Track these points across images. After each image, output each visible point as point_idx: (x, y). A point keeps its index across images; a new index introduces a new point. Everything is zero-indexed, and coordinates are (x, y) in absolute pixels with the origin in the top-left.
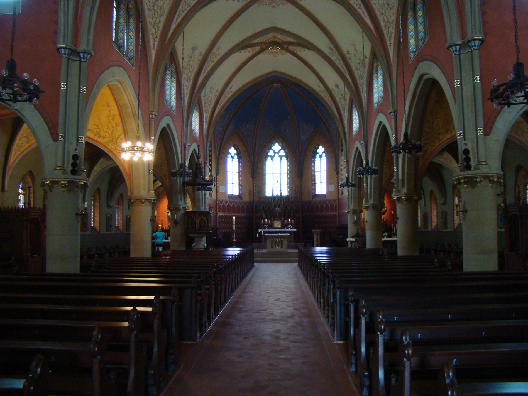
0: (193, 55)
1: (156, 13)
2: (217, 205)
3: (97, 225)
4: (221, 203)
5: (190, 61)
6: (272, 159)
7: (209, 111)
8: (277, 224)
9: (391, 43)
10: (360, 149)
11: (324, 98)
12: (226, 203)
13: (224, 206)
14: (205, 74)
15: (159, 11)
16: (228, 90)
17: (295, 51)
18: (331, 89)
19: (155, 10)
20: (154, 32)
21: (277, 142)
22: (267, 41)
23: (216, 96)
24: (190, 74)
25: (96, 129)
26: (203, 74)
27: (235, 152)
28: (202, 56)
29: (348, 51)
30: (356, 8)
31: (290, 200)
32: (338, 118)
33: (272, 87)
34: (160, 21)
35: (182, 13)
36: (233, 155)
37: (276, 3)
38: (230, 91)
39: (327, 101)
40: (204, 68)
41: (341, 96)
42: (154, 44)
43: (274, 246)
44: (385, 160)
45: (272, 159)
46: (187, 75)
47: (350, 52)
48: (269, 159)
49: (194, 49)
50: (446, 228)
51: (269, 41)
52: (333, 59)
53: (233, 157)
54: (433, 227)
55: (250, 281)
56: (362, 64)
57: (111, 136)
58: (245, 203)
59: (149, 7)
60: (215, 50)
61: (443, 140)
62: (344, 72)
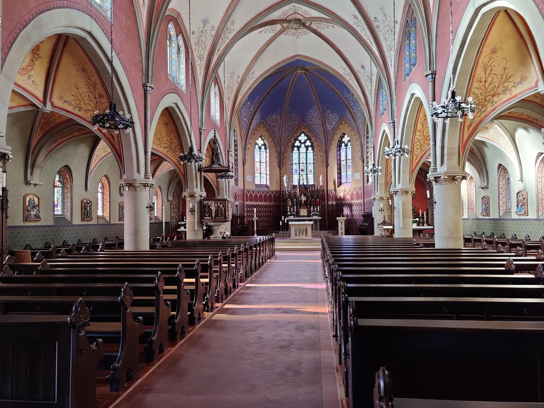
0: (205, 29)
2: (244, 195)
3: (107, 215)
4: (249, 192)
5: (201, 36)
6: (298, 150)
8: (304, 212)
10: (387, 131)
11: (350, 82)
12: (254, 192)
13: (251, 195)
14: (220, 52)
16: (250, 76)
17: (318, 30)
18: (357, 71)
23: (238, 82)
25: (74, 100)
29: (375, 18)
31: (316, 189)
33: (296, 74)
38: (252, 77)
39: (352, 84)
41: (367, 78)
43: (298, 235)
44: (416, 140)
45: (298, 150)
47: (378, 19)
48: (296, 149)
50: (488, 215)
52: (358, 29)
53: (260, 148)
55: (261, 274)
56: (392, 31)
58: (272, 192)
61: (498, 103)
62: (370, 44)
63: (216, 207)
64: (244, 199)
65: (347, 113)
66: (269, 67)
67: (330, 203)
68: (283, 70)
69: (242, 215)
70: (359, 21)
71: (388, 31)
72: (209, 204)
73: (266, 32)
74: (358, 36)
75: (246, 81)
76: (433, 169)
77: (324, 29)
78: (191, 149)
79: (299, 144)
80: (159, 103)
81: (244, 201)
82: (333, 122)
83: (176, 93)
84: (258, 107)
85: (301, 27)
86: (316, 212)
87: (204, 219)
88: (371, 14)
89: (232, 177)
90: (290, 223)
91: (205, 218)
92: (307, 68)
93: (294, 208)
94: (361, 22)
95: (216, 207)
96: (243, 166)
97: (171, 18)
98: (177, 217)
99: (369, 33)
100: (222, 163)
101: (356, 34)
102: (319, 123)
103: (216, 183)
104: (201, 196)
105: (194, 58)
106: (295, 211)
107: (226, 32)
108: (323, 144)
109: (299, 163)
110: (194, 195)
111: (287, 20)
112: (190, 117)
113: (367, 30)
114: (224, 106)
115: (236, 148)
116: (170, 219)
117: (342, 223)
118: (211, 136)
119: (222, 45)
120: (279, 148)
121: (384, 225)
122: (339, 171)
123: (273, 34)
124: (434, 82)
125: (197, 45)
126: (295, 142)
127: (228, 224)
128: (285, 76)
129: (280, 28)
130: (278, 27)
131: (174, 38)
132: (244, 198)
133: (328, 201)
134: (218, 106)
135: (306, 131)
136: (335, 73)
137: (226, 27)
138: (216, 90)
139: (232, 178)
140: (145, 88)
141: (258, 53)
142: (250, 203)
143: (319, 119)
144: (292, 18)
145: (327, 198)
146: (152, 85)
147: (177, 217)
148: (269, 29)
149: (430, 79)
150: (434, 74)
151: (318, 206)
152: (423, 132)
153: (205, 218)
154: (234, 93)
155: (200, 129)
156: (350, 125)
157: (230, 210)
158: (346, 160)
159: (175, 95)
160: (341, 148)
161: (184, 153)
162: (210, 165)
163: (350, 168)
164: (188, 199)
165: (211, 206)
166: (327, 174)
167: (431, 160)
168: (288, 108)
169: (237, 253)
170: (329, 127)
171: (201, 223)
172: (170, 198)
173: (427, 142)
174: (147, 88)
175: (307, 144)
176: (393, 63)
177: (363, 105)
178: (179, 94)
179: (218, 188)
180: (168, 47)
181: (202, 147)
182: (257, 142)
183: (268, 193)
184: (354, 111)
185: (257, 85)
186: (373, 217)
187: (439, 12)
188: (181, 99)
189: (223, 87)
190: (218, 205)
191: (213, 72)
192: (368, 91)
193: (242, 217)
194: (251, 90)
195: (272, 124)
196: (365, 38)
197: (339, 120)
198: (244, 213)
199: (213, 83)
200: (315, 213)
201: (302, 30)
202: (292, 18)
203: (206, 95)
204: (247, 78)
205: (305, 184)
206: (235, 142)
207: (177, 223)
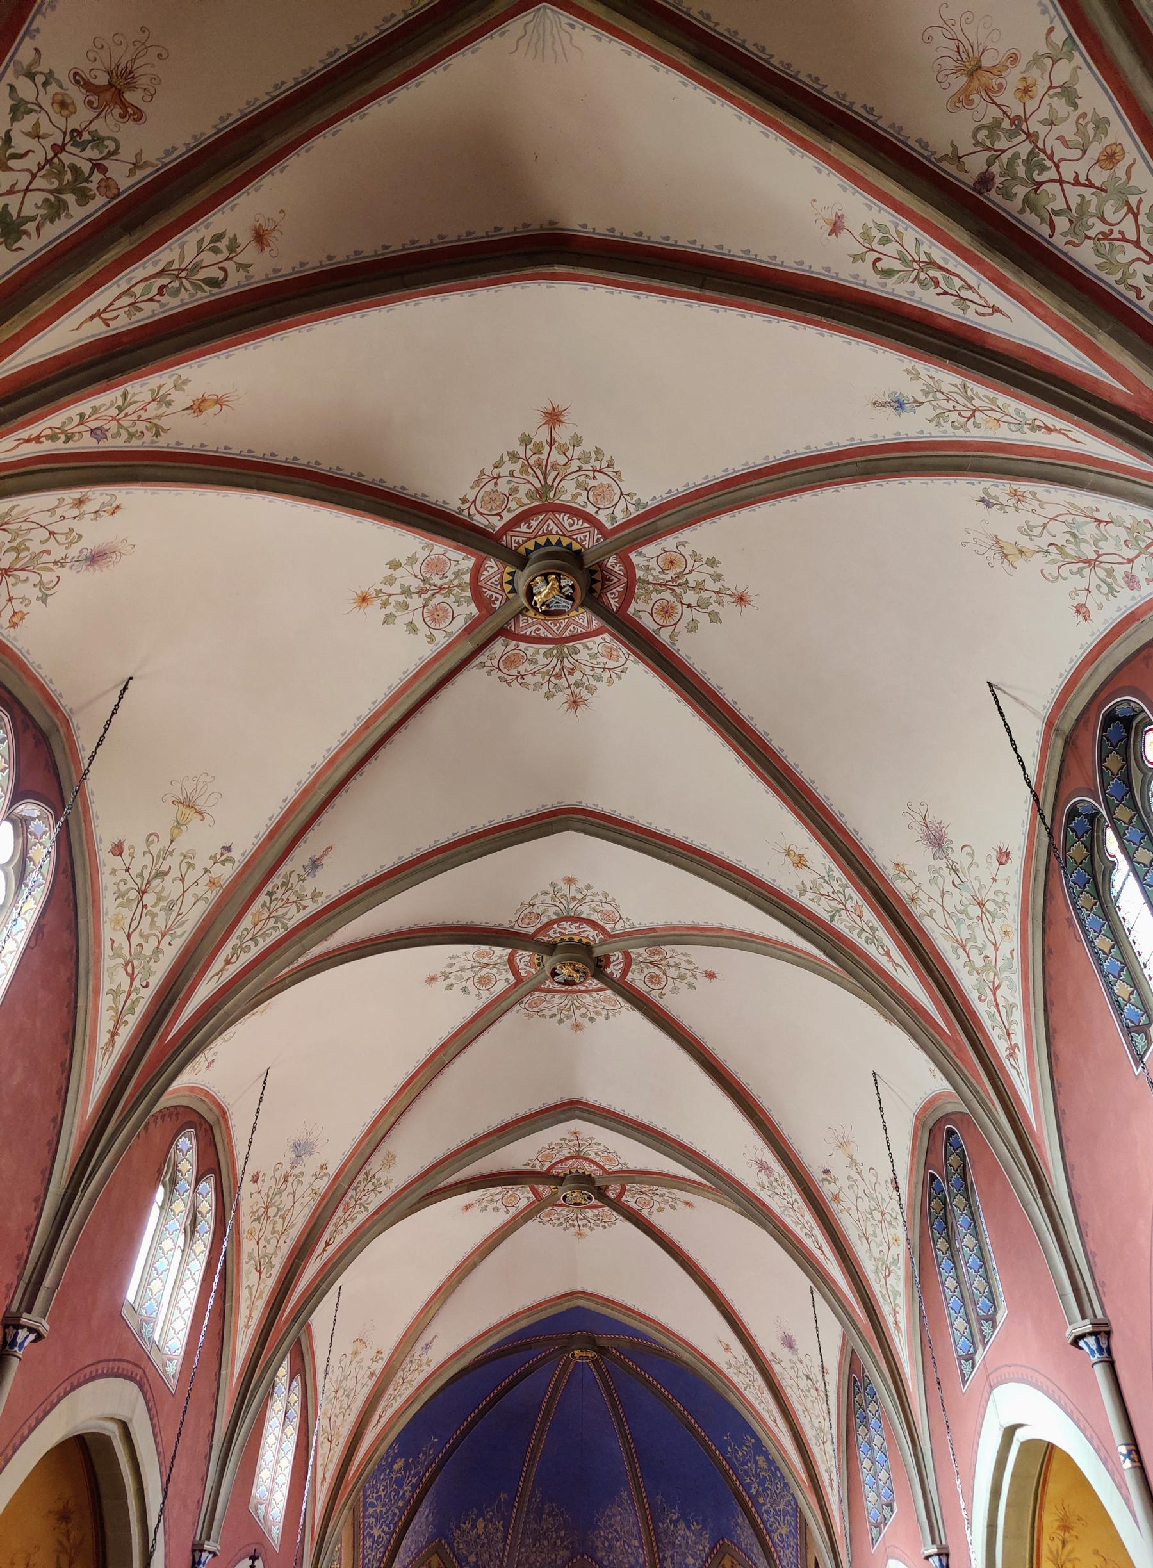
0: (296, 1171)
1: (146, 920)
5: (280, 1192)
7: (339, 1435)
9: (1017, 1045)
14: (331, 1249)
15: (162, 916)
16: (417, 1357)
17: (645, 1213)
18: (769, 1357)
20: (125, 986)
23: (372, 1374)
26: (324, 1250)
29: (826, 1172)
30: (861, 942)
32: (803, 1475)
34: (158, 950)
35: (252, 943)
37: (583, 1010)
38: (425, 1358)
39: (756, 1404)
41: (804, 1383)
42: (114, 1034)
46: (332, 1420)
49: (301, 1149)
59: (123, 888)
62: (817, 1253)
65: (737, 1524)
66: (484, 1327)
68: (529, 1343)
70: (776, 1180)
73: (485, 1208)
74: (776, 1227)
75: (400, 1373)
77: (661, 1210)
80: (53, 1406)
84: (431, 1480)
85: (594, 1201)
88: (813, 1158)
92: (603, 1343)
94: (783, 1183)
97: (194, 1118)
99: (809, 1218)
101: (771, 1221)
102: (641, 1561)
105: (239, 1263)
111: (553, 1176)
113: (804, 1206)
114: (311, 1460)
123: (507, 1217)
124: (1111, 1365)
125: (259, 1218)
128: (530, 1367)
129: (528, 1198)
130: (523, 1196)
131: (185, 1183)
136: (699, 1360)
137: (363, 1172)
138: (293, 1398)
140: (11, 1331)
141: (451, 1276)
143: (640, 1542)
146: (44, 1323)
148: (496, 1198)
149: (1092, 1351)
150: (1102, 1333)
154: (351, 1418)
155: (197, 1549)
159: (131, 1388)
168: (533, 1495)
174: (16, 1334)
176: (902, 1318)
178: (146, 1387)
180: (155, 1212)
184: (765, 1516)
185: (434, 1391)
187: (1062, 1124)
188: (149, 1409)
189: (320, 1389)
191: (295, 1320)
192: (814, 1432)
196: (801, 1233)
199: (286, 1363)
201: (598, 1212)
202: (568, 1172)
204: (408, 1360)
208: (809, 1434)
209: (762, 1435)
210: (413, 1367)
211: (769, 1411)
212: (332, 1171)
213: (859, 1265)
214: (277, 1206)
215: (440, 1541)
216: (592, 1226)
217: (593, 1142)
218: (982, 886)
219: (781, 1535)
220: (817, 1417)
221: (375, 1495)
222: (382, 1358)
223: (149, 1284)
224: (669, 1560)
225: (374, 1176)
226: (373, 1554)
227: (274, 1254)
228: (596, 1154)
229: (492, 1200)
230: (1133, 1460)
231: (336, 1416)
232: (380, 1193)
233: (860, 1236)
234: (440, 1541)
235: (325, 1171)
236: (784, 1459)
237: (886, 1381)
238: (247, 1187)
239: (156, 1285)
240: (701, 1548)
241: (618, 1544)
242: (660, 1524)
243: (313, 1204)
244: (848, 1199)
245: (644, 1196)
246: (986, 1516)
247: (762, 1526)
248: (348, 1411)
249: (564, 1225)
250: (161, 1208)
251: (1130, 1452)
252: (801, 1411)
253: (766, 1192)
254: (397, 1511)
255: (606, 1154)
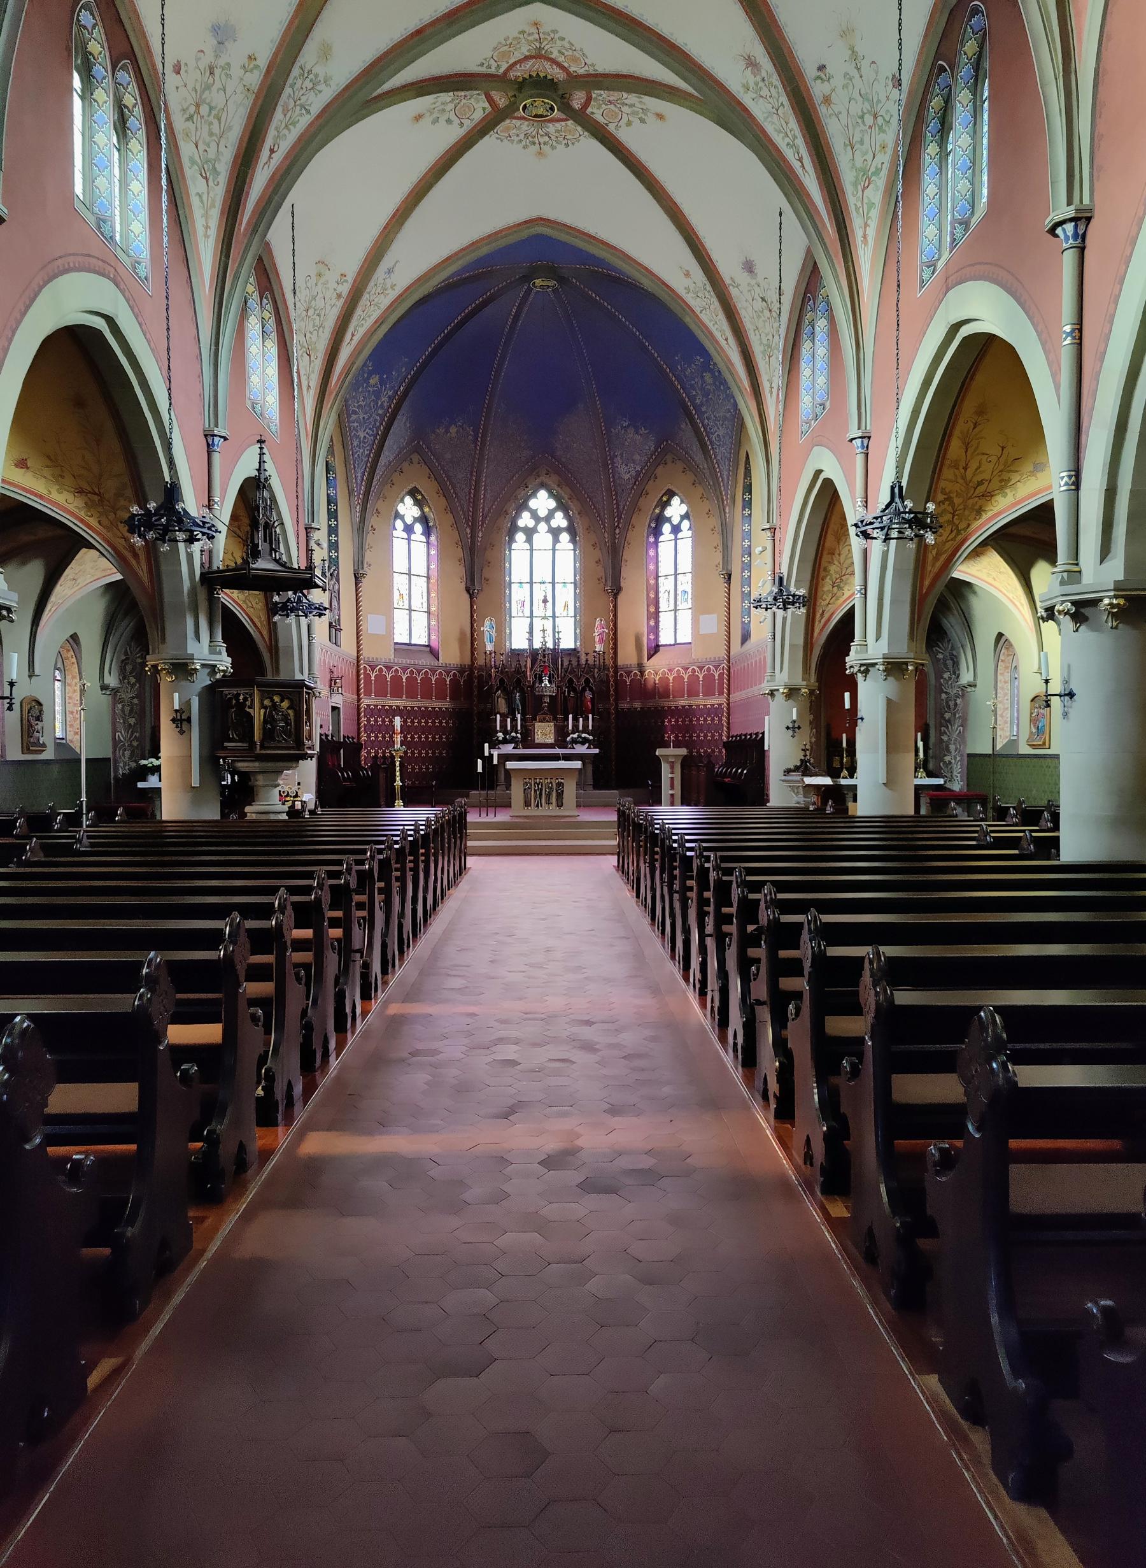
2: (358, 675)
5: (208, 87)
6: (529, 540)
8: (544, 732)
11: (703, 316)
13: (381, 677)
14: (278, 157)
16: (381, 281)
17: (611, 128)
18: (728, 281)
19: (202, 117)
21: (543, 486)
22: (512, 75)
23: (339, 296)
24: (213, 145)
27: (416, 512)
28: (256, 72)
29: (822, 68)
31: (583, 662)
33: (529, 290)
36: (409, 521)
38: (389, 283)
39: (710, 325)
40: (271, 133)
41: (759, 304)
45: (529, 540)
48: (520, 537)
49: (222, 33)
51: (519, 73)
53: (409, 529)
54: (999, 747)
57: (96, 490)
60: (309, 55)
62: (796, 165)
63: (266, 708)
64: (358, 690)
67: (624, 705)
69: (353, 738)
71: (864, 114)
72: (241, 697)
76: (1065, 574)
78: (172, 492)
79: (531, 523)
81: (358, 695)
82: (637, 457)
83: (109, 278)
84: (405, 394)
86: (583, 732)
87: (225, 748)
88: (807, 57)
89: (320, 611)
90: (510, 765)
91: (226, 744)
93: (514, 720)
94: (771, 83)
95: (266, 708)
96: (356, 584)
98: (135, 744)
100: (284, 558)
103: (265, 633)
104: (213, 669)
106: (519, 728)
107: (299, 82)
108: (603, 523)
109: (531, 583)
110: (186, 664)
112: (166, 374)
113: (791, 112)
115: (333, 523)
116: (111, 750)
117: (672, 768)
118: (246, 467)
119: (286, 132)
120: (468, 531)
121: (804, 775)
122: (652, 610)
123: (462, 132)
124: (1082, 250)
125: (191, 117)
126: (518, 515)
127: (308, 769)
130: (477, 106)
132: (358, 686)
133: (617, 700)
134: (273, 370)
135: (552, 480)
138: (267, 315)
139: (320, 615)
142: (380, 702)
144: (527, 76)
145: (616, 690)
147: (135, 744)
151: (590, 716)
152: (965, 469)
153: (226, 744)
156: (690, 466)
157: (316, 719)
158: (676, 574)
160: (660, 540)
161: (142, 506)
162: (246, 562)
163: (686, 600)
164: (166, 680)
165: (248, 703)
166: (615, 616)
167: (858, 602)
169: (353, 884)
170: (626, 472)
171: (211, 762)
172: (112, 680)
173: (974, 505)
175: (554, 523)
176: (871, 232)
177: (741, 393)
179: (274, 649)
180: (77, 103)
181: (217, 499)
182: (401, 508)
183: (433, 672)
186: (766, 748)
190: (272, 700)
191: (254, 231)
193: (354, 748)
194: (385, 329)
195: (448, 456)
196: (781, 142)
197: (656, 450)
198: (359, 733)
200: (579, 736)
202: (527, 76)
203: (228, 308)
205: (550, 645)
206: (329, 504)
207: (136, 762)
208: (757, 349)
209: (712, 351)
210: (379, 290)
211: (722, 332)
212: (263, 61)
213: (839, 178)
214: (209, 104)
215: (419, 442)
216: (554, 144)
217: (557, 36)
218: (879, 101)
219: (718, 435)
220: (767, 335)
221: (356, 405)
222: (346, 281)
223: (93, 182)
224: (619, 457)
225: (310, 72)
226: (361, 451)
227: (217, 159)
228: (560, 52)
229: (444, 110)
230: (1074, 338)
231: (311, 333)
232: (320, 92)
233: (845, 145)
234: (419, 442)
235: (254, 63)
236: (730, 372)
237: (843, 294)
238: (171, 81)
239: (101, 182)
240: (647, 448)
241: (575, 445)
242: (612, 429)
243: (249, 103)
244: (840, 100)
245: (612, 107)
246: (914, 403)
247: (702, 429)
248: (321, 329)
249: (524, 143)
250: (82, 98)
251: (1073, 330)
252: (752, 330)
253: (751, 94)
254: (378, 418)
255: (570, 53)
